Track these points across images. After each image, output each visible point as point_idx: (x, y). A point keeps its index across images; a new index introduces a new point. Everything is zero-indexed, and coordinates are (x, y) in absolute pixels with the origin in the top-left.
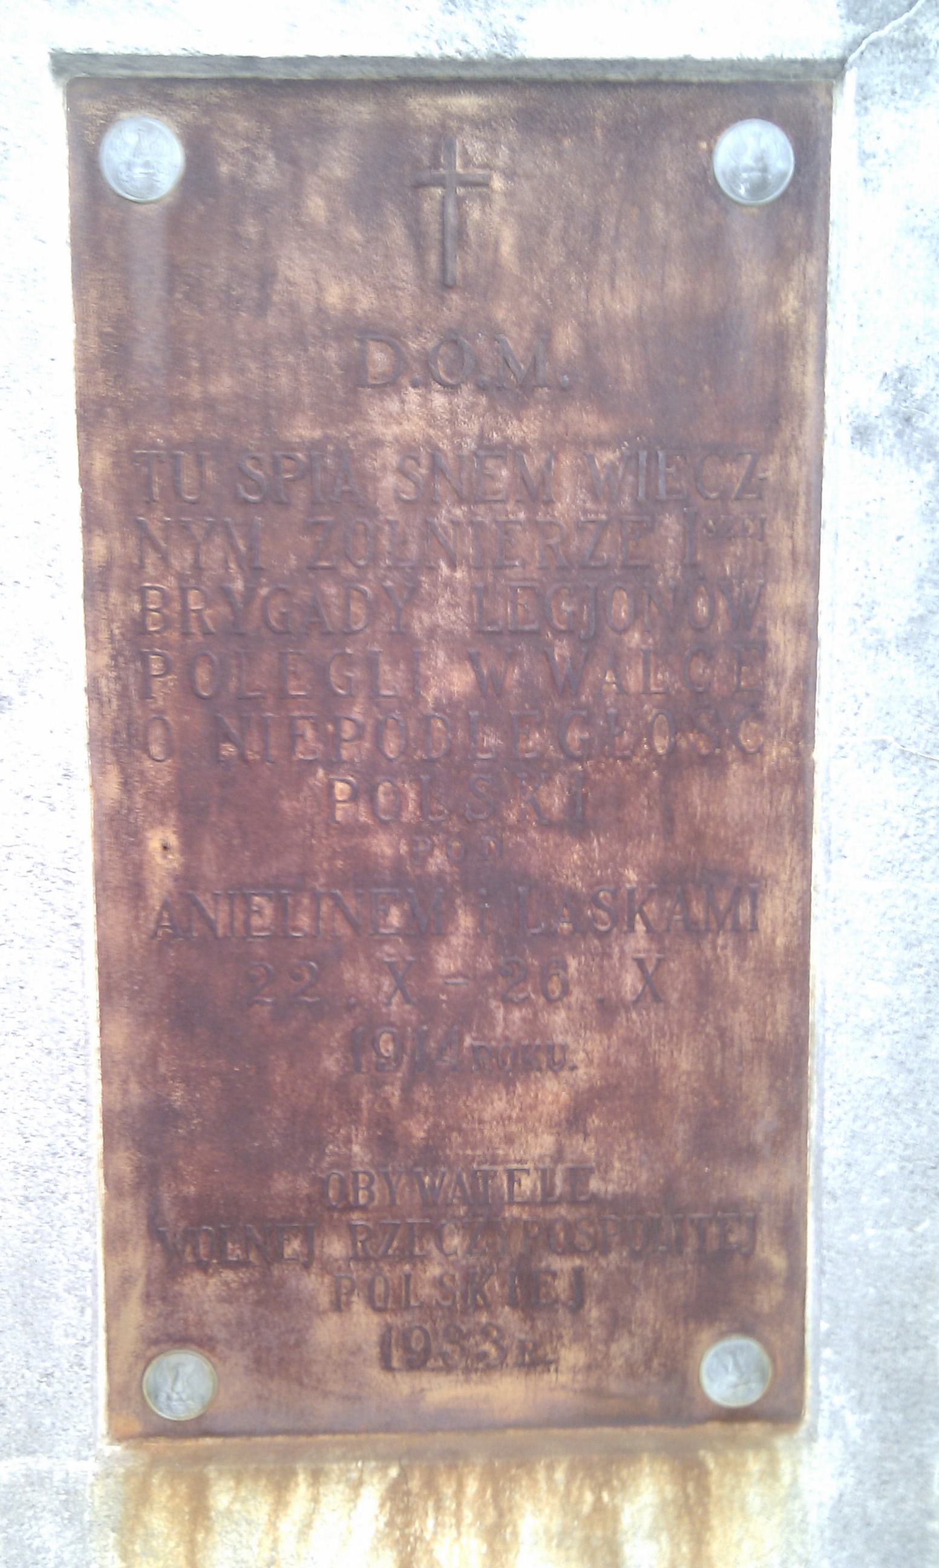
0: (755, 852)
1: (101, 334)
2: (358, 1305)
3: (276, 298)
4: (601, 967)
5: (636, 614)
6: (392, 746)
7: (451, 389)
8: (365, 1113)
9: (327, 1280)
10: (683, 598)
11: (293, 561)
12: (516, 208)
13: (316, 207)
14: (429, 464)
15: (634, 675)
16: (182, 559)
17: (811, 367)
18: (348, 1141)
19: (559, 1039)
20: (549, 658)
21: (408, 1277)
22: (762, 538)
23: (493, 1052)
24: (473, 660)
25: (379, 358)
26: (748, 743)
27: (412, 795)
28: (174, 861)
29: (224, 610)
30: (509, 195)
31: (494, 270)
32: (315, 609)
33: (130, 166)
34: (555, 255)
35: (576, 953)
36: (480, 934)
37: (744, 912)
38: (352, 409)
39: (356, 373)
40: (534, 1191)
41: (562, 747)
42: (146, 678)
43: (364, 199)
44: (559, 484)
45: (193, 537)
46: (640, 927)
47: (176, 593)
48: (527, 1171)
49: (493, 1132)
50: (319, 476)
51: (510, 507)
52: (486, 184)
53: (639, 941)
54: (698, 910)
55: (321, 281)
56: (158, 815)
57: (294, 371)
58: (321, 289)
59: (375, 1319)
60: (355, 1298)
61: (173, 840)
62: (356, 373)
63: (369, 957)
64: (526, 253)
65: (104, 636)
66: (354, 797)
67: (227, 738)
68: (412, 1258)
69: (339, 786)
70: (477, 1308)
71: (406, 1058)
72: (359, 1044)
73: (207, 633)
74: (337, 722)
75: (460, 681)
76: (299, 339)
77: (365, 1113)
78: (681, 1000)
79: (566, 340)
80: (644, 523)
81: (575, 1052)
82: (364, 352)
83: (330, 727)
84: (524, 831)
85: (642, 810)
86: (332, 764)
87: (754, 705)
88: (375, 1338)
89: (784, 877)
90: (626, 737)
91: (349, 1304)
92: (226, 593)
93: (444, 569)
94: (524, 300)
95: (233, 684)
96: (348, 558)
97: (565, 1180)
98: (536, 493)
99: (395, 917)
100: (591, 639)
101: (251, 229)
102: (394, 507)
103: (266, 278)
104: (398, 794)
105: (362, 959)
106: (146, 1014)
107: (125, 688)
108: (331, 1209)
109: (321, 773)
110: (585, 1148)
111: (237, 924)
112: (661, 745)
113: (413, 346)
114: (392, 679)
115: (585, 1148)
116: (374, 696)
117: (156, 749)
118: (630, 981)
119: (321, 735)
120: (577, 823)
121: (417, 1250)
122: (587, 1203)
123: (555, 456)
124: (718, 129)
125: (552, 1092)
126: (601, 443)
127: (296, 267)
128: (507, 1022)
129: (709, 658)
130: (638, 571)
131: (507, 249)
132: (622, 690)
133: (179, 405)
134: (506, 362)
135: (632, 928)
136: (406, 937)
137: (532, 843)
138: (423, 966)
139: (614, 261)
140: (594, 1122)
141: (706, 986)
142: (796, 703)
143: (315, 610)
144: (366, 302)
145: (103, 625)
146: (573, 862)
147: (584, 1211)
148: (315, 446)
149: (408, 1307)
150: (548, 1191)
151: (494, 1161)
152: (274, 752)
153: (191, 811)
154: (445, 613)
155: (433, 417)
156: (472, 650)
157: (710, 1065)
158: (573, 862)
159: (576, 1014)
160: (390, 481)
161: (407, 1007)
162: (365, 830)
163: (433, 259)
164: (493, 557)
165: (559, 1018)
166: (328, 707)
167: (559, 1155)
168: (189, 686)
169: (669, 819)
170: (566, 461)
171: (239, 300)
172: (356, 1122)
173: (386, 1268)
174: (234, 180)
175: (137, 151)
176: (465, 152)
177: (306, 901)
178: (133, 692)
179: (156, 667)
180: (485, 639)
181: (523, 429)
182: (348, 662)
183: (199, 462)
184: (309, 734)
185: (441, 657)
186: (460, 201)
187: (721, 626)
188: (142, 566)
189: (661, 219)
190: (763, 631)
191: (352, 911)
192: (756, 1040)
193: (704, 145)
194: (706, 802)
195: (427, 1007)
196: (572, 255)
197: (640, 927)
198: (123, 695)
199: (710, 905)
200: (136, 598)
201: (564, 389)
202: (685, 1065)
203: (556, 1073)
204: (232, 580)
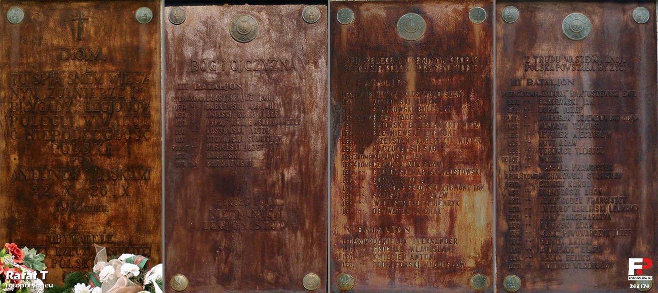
0: (149, 161)
1: (5, 50)
2: (57, 266)
3: (43, 42)
4: (114, 188)
5: (121, 108)
6: (66, 137)
7: (80, 60)
8: (59, 221)
9: (50, 260)
10: (132, 105)
11: (45, 97)
12: (94, 24)
13: (51, 24)
14: (76, 77)
15: (121, 121)
16: (21, 96)
17: (158, 56)
18: (55, 227)
19: (105, 204)
20: (101, 117)
21: (69, 260)
22: (149, 91)
23: (89, 207)
24: (85, 118)
25: (65, 54)
26: (147, 137)
27: (71, 147)
28: (17, 162)
29: (29, 107)
30: (93, 22)
31: (89, 36)
32: (50, 106)
33: (13, 17)
34: (102, 34)
35: (108, 184)
36: (86, 180)
37: (147, 175)
38: (59, 65)
39: (59, 58)
40: (99, 240)
41: (105, 137)
42: (12, 122)
43: (62, 23)
44: (103, 80)
45: (23, 91)
46: (123, 179)
47: (19, 103)
48: (97, 235)
49: (89, 226)
50: (51, 78)
51: (93, 85)
52: (88, 19)
53: (123, 181)
54: (136, 175)
55: (52, 39)
56: (13, 151)
57: (46, 57)
58: (52, 41)
59: (61, 270)
60: (57, 265)
61: (17, 157)
62: (59, 58)
63: (60, 184)
64: (96, 33)
65: (3, 112)
66: (58, 148)
67: (29, 135)
68: (70, 255)
69: (54, 145)
70: (85, 268)
71: (69, 208)
72: (58, 205)
73: (26, 112)
74: (54, 131)
75: (82, 122)
76: (47, 50)
77: (59, 221)
78: (133, 195)
79: (105, 50)
80: (123, 89)
81: (108, 207)
82: (61, 53)
83: (52, 133)
84: (96, 156)
85: (123, 151)
86: (53, 141)
87: (148, 127)
88: (61, 274)
89: (156, 167)
90: (119, 135)
91: (55, 266)
92: (30, 103)
93: (78, 98)
94: (96, 42)
95: (31, 123)
96: (57, 96)
97: (106, 238)
98: (98, 82)
99: (67, 176)
100: (111, 114)
101: (38, 29)
102: (67, 85)
103: (41, 38)
104: (68, 147)
105: (59, 184)
106: (9, 196)
107: (7, 124)
108: (52, 243)
109: (50, 142)
110: (110, 230)
111: (31, 176)
112: (127, 137)
113: (72, 52)
114: (66, 122)
115: (110, 230)
116: (63, 126)
117: (13, 137)
118: (121, 191)
119: (50, 134)
120: (109, 154)
121: (71, 254)
122: (111, 243)
123: (103, 74)
124: (137, 9)
125: (103, 217)
126: (113, 72)
127: (47, 36)
128: (92, 200)
129: (138, 118)
130: (121, 99)
131: (92, 32)
132: (119, 125)
133: (22, 64)
134: (92, 55)
135: (121, 179)
136: (69, 180)
137: (98, 158)
138: (72, 187)
139: (115, 35)
140: (113, 224)
141: (139, 193)
142: (157, 128)
143: (49, 107)
144: (62, 43)
145: (3, 110)
146: (107, 163)
147: (111, 245)
148: (50, 72)
149: (69, 267)
150: (102, 240)
151: (89, 233)
152: (40, 138)
153: (21, 151)
154: (78, 107)
155: (76, 66)
156: (85, 116)
157: (139, 211)
158: (107, 163)
159: (108, 198)
160: (66, 79)
161: (69, 196)
162: (60, 155)
163: (76, 35)
164: (89, 97)
165: (105, 199)
166: (52, 128)
167: (105, 232)
168: (21, 123)
169: (129, 153)
170: (105, 75)
171: (35, 43)
172: (58, 223)
173: (64, 258)
174: (34, 19)
175: (15, 14)
176: (83, 13)
177: (46, 171)
178: (9, 124)
179: (14, 119)
180: (88, 113)
181: (96, 68)
182: (57, 118)
183: (25, 75)
184: (48, 134)
185: (77, 117)
186: (82, 23)
187: (140, 111)
188: (12, 98)
189: (125, 27)
190: (149, 112)
191: (57, 174)
192: (150, 205)
193: (133, 12)
194: (138, 150)
195: (74, 197)
196: (106, 33)
197: (123, 179)
198: (7, 125)
199: (139, 173)
200: (10, 104)
201: (105, 60)
202: (134, 211)
203: (104, 212)
204: (32, 100)
